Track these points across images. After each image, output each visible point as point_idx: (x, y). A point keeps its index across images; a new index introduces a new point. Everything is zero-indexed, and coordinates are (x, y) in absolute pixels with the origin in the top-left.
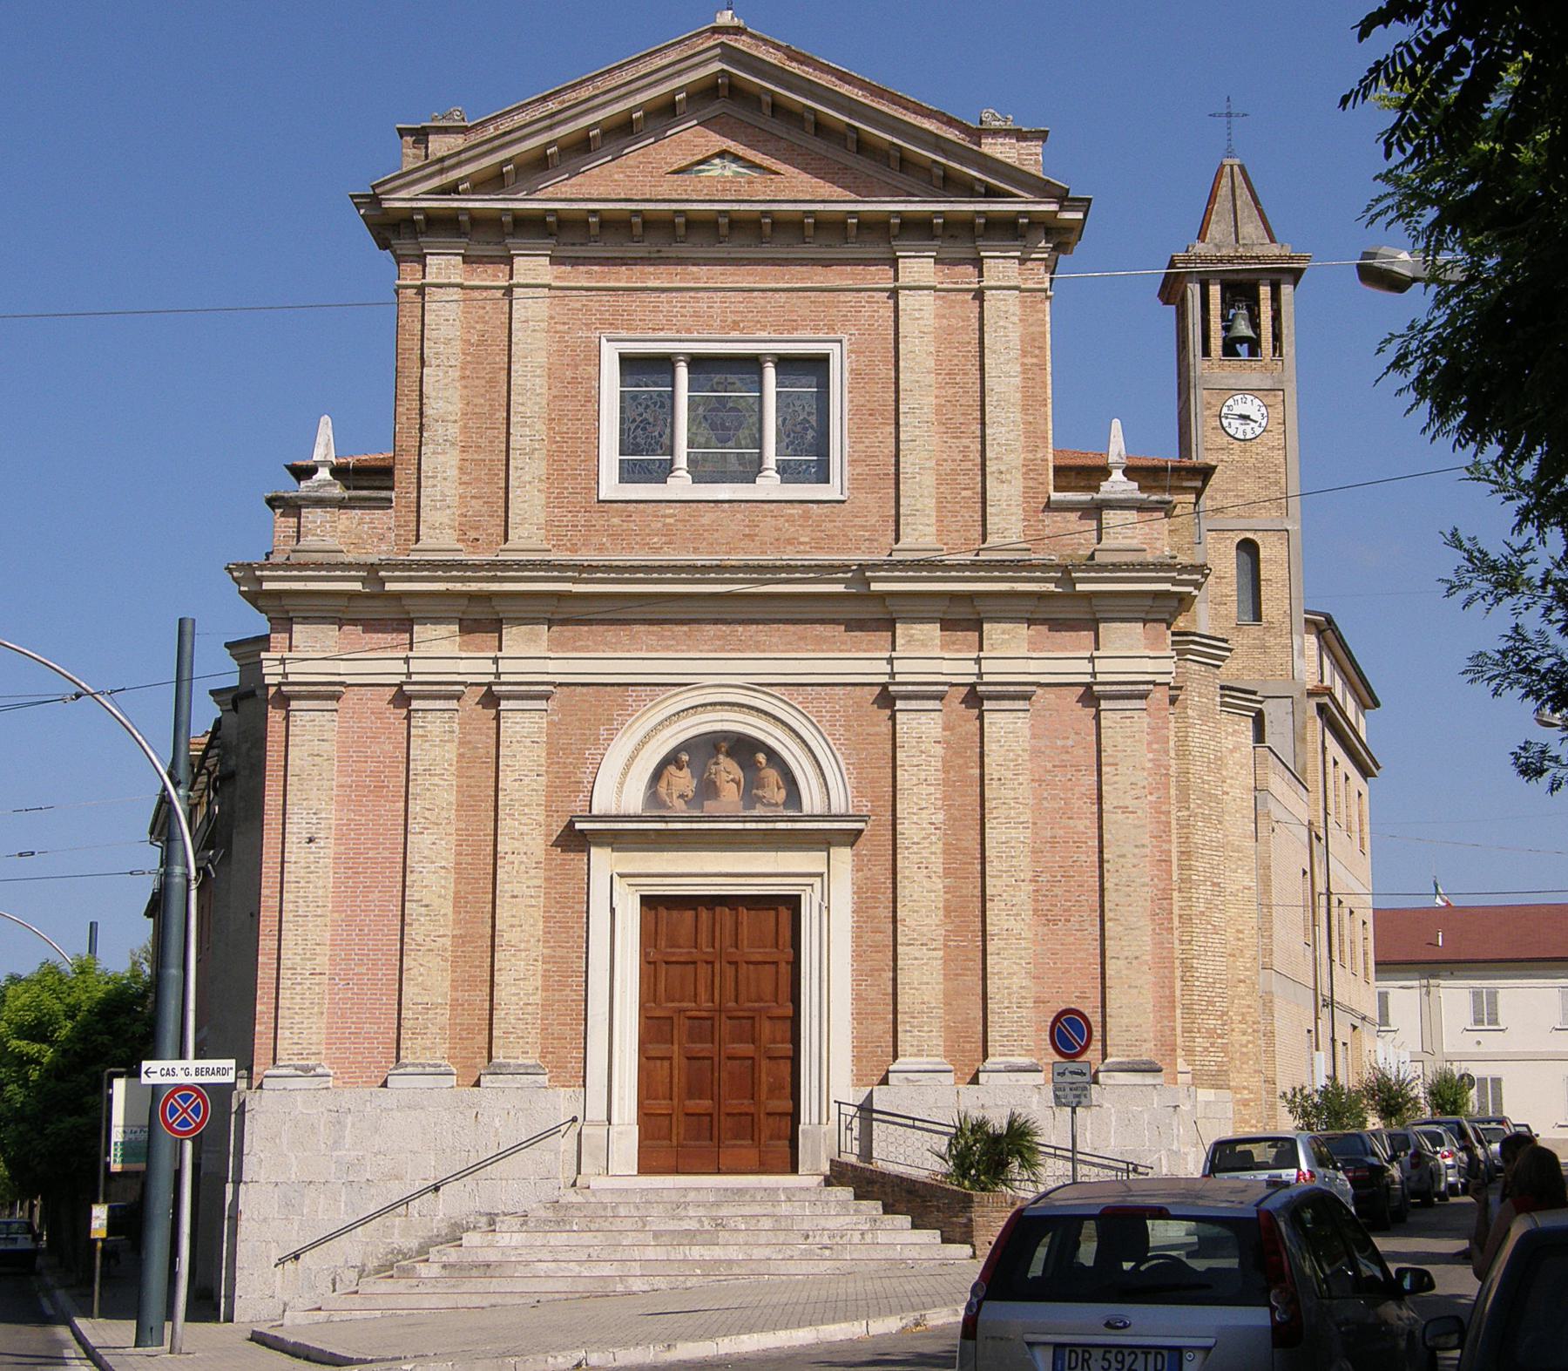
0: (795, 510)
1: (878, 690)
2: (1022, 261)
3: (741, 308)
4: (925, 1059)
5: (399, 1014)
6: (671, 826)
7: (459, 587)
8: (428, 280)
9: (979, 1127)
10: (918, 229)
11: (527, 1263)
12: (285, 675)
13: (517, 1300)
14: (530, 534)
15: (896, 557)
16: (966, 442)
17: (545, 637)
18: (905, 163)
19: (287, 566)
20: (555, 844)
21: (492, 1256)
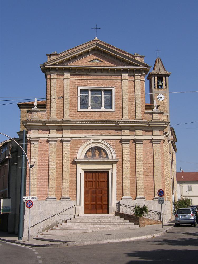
0: (107, 113)
1: (120, 140)
2: (141, 76)
3: (99, 82)
4: (128, 196)
5: (48, 189)
6: (89, 161)
7: (57, 124)
8: (52, 78)
9: (139, 207)
10: (125, 71)
11: (73, 227)
12: (30, 137)
13: (72, 233)
14: (67, 116)
15: (122, 120)
16: (133, 103)
17: (70, 132)
18: (123, 61)
19: (31, 121)
20: (71, 163)
21: (67, 226)
